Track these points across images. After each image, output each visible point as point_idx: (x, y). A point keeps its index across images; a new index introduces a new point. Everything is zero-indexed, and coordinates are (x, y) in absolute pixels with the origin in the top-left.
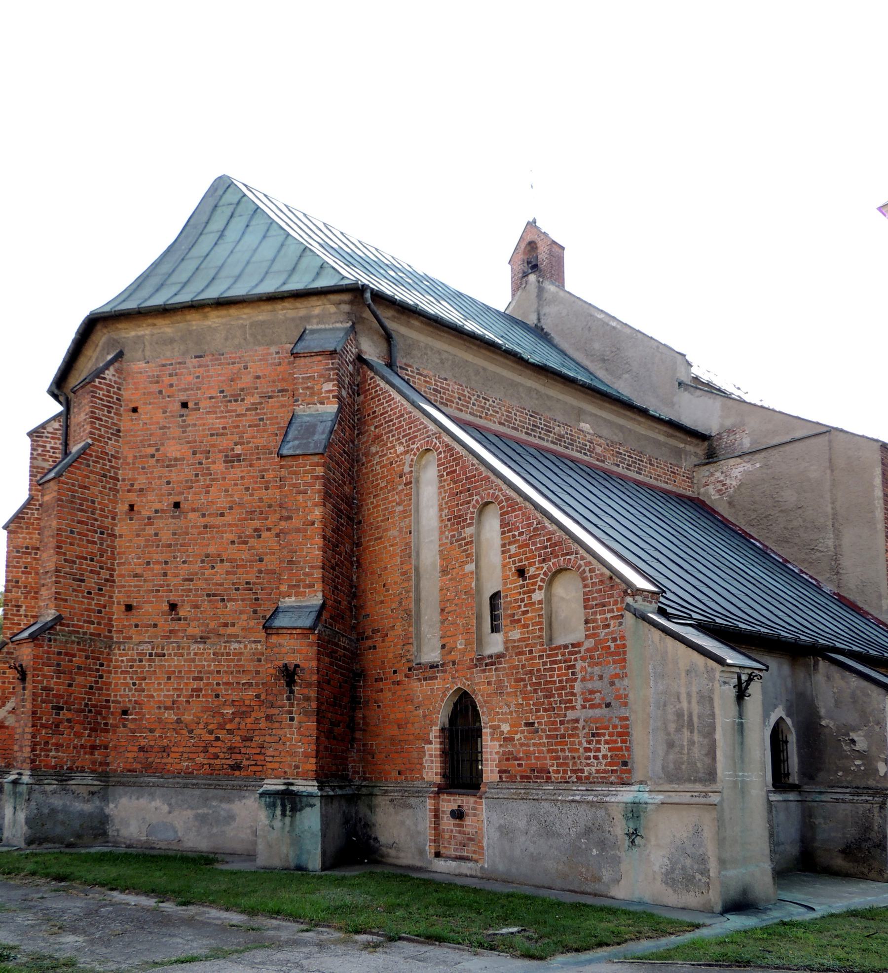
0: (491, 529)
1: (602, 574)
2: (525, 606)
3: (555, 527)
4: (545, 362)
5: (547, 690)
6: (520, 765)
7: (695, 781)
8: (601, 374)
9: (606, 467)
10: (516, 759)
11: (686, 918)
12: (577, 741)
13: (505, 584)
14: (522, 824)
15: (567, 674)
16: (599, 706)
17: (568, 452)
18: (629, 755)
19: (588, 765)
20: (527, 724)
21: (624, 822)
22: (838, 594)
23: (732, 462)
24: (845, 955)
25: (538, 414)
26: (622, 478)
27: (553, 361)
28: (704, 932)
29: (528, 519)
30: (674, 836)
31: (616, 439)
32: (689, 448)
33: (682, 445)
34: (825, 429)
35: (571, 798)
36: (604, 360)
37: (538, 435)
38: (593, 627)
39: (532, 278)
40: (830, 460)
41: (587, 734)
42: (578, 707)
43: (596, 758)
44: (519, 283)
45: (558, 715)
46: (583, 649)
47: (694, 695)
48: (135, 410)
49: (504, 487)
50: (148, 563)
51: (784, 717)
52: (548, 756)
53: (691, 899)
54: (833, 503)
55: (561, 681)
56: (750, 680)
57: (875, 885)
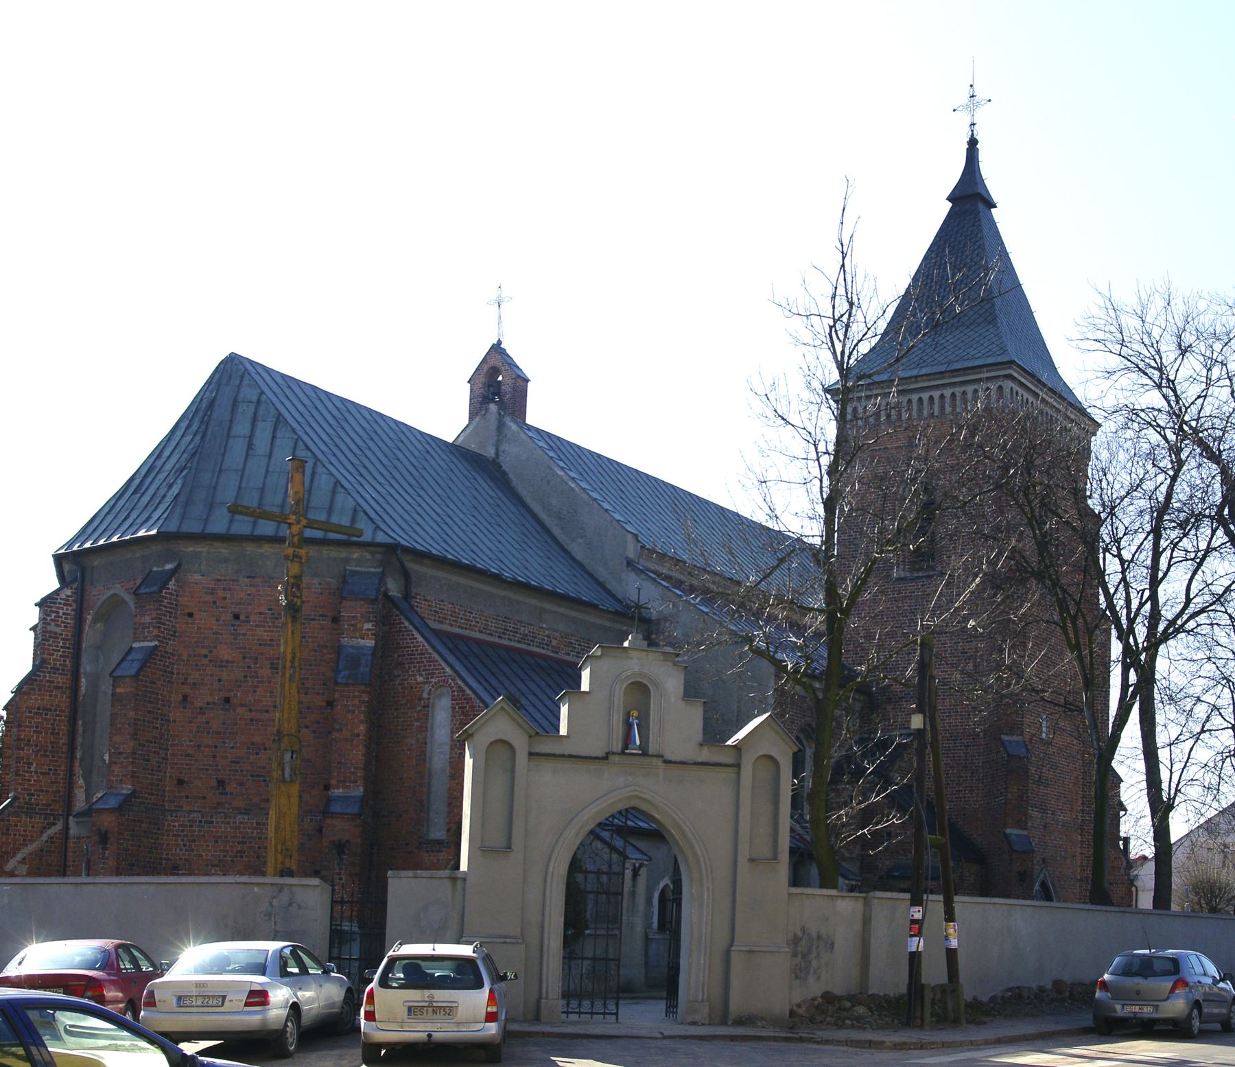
17: (530, 648)
44: (478, 405)
48: (190, 615)
50: (199, 746)
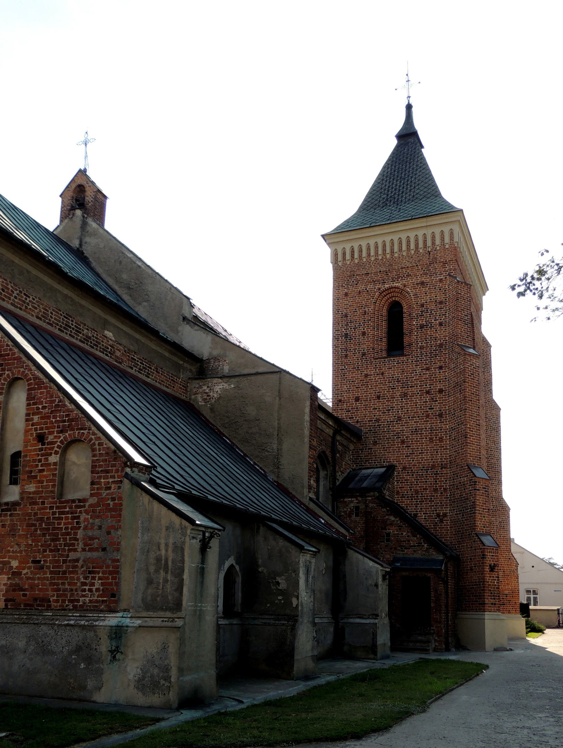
0: (19, 400)
1: (108, 448)
2: (42, 465)
3: (73, 407)
4: (81, 278)
5: (54, 534)
6: (25, 595)
7: (166, 610)
8: (126, 297)
9: (122, 367)
10: (22, 590)
11: (151, 714)
12: (76, 577)
13: (26, 446)
14: (21, 644)
15: (72, 523)
16: (96, 550)
18: (117, 589)
19: (83, 596)
20: (33, 562)
21: (109, 641)
22: (277, 482)
23: (215, 380)
24: (259, 734)
25: (71, 317)
26: (132, 376)
27: (88, 279)
28: (163, 724)
29: (52, 396)
30: (147, 652)
31: (132, 348)
32: (186, 365)
33: (181, 362)
34: (278, 370)
35: (66, 622)
36: (129, 288)
37: (69, 332)
38: (98, 488)
39: (79, 212)
40: (279, 390)
41: (85, 571)
42: (79, 550)
43: (90, 590)
44: (67, 213)
45: (62, 556)
46: (87, 504)
47: (171, 545)
49: (33, 368)
51: (234, 564)
52: (50, 588)
53: (156, 699)
54: (279, 420)
55: (66, 528)
56: (211, 537)
57: (285, 682)
